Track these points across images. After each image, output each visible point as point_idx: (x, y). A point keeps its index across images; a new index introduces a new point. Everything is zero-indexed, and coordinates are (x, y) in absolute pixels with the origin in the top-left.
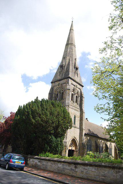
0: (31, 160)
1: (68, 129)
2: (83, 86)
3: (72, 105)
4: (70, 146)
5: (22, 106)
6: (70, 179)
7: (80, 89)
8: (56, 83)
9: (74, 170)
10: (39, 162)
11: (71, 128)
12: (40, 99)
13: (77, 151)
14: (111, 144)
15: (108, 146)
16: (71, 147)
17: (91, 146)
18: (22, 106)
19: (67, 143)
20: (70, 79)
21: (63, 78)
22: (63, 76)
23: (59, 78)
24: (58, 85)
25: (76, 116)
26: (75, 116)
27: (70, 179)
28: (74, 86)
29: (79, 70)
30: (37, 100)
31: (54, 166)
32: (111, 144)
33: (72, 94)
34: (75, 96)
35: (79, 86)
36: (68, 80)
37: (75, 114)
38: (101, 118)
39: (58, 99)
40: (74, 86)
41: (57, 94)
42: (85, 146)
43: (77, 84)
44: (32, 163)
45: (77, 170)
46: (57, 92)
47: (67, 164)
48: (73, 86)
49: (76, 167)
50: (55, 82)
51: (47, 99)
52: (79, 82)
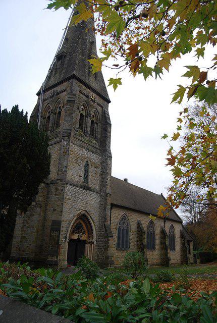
5: (27, 113)
6: (210, 32)
7: (102, 107)
12: (173, 59)
13: (93, 243)
14: (172, 227)
15: (168, 232)
16: (78, 233)
18: (27, 113)
20: (75, 81)
23: (53, 81)
25: (90, 163)
26: (88, 165)
27: (210, 32)
32: (172, 227)
33: (82, 115)
34: (89, 121)
35: (98, 99)
38: (165, 136)
41: (49, 117)
46: (49, 112)
48: (84, 97)
52: (99, 90)
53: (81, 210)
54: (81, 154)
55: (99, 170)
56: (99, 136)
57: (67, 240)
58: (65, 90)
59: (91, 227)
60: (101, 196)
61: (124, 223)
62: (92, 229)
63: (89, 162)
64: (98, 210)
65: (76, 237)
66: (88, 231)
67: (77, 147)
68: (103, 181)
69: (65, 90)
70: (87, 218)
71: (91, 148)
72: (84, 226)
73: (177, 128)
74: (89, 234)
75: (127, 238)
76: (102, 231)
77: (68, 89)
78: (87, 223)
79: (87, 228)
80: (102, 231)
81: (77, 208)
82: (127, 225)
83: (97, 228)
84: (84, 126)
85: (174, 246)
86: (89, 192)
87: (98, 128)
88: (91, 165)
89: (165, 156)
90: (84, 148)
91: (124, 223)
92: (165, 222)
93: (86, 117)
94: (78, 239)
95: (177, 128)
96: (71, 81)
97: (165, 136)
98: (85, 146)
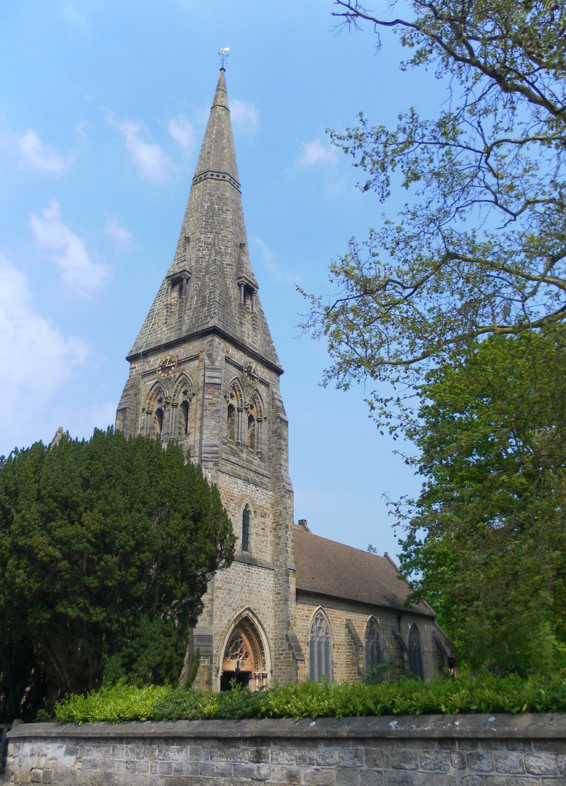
0: (27, 748)
1: (213, 568)
2: (279, 372)
3: (233, 459)
4: (226, 655)
8: (152, 359)
9: (248, 773)
10: (69, 752)
11: (228, 564)
13: (265, 676)
15: (406, 642)
16: (233, 657)
17: (327, 644)
19: (215, 642)
20: (217, 340)
21: (184, 334)
22: (185, 328)
23: (165, 335)
24: (157, 482)
25: (251, 508)
28: (240, 368)
29: (261, 293)
30: (97, 432)
31: (145, 762)
35: (261, 371)
36: (211, 344)
37: (247, 501)
39: (360, 780)
40: (240, 368)
42: (299, 649)
43: (255, 365)
44: (30, 762)
45: (264, 771)
47: (215, 743)
48: (235, 371)
49: (258, 758)
50: (146, 354)
51: (87, 439)
53: (242, 607)
54: (236, 491)
55: (269, 521)
56: (265, 448)
57: (220, 674)
58: (196, 357)
59: (260, 642)
60: (276, 576)
61: (319, 628)
62: (262, 648)
63: (250, 505)
64: (271, 604)
65: (232, 666)
66: (255, 651)
67: (227, 478)
68: (277, 544)
69: (196, 357)
70: (252, 625)
71: (252, 475)
72: (247, 642)
73: (336, 291)
74: (256, 657)
75: (327, 660)
76: (283, 651)
77: (204, 355)
78: (251, 632)
79: (253, 645)
80: (283, 651)
81: (234, 606)
82: (327, 633)
83: (272, 645)
84: (236, 430)
85: (421, 667)
86: (254, 569)
87: (264, 431)
88: (255, 512)
89: (398, 114)
90: (239, 477)
91: (319, 628)
92: (399, 619)
93: (239, 411)
94: (237, 669)
95: (336, 291)
96: (210, 338)
97: (396, 452)
98: (242, 472)
